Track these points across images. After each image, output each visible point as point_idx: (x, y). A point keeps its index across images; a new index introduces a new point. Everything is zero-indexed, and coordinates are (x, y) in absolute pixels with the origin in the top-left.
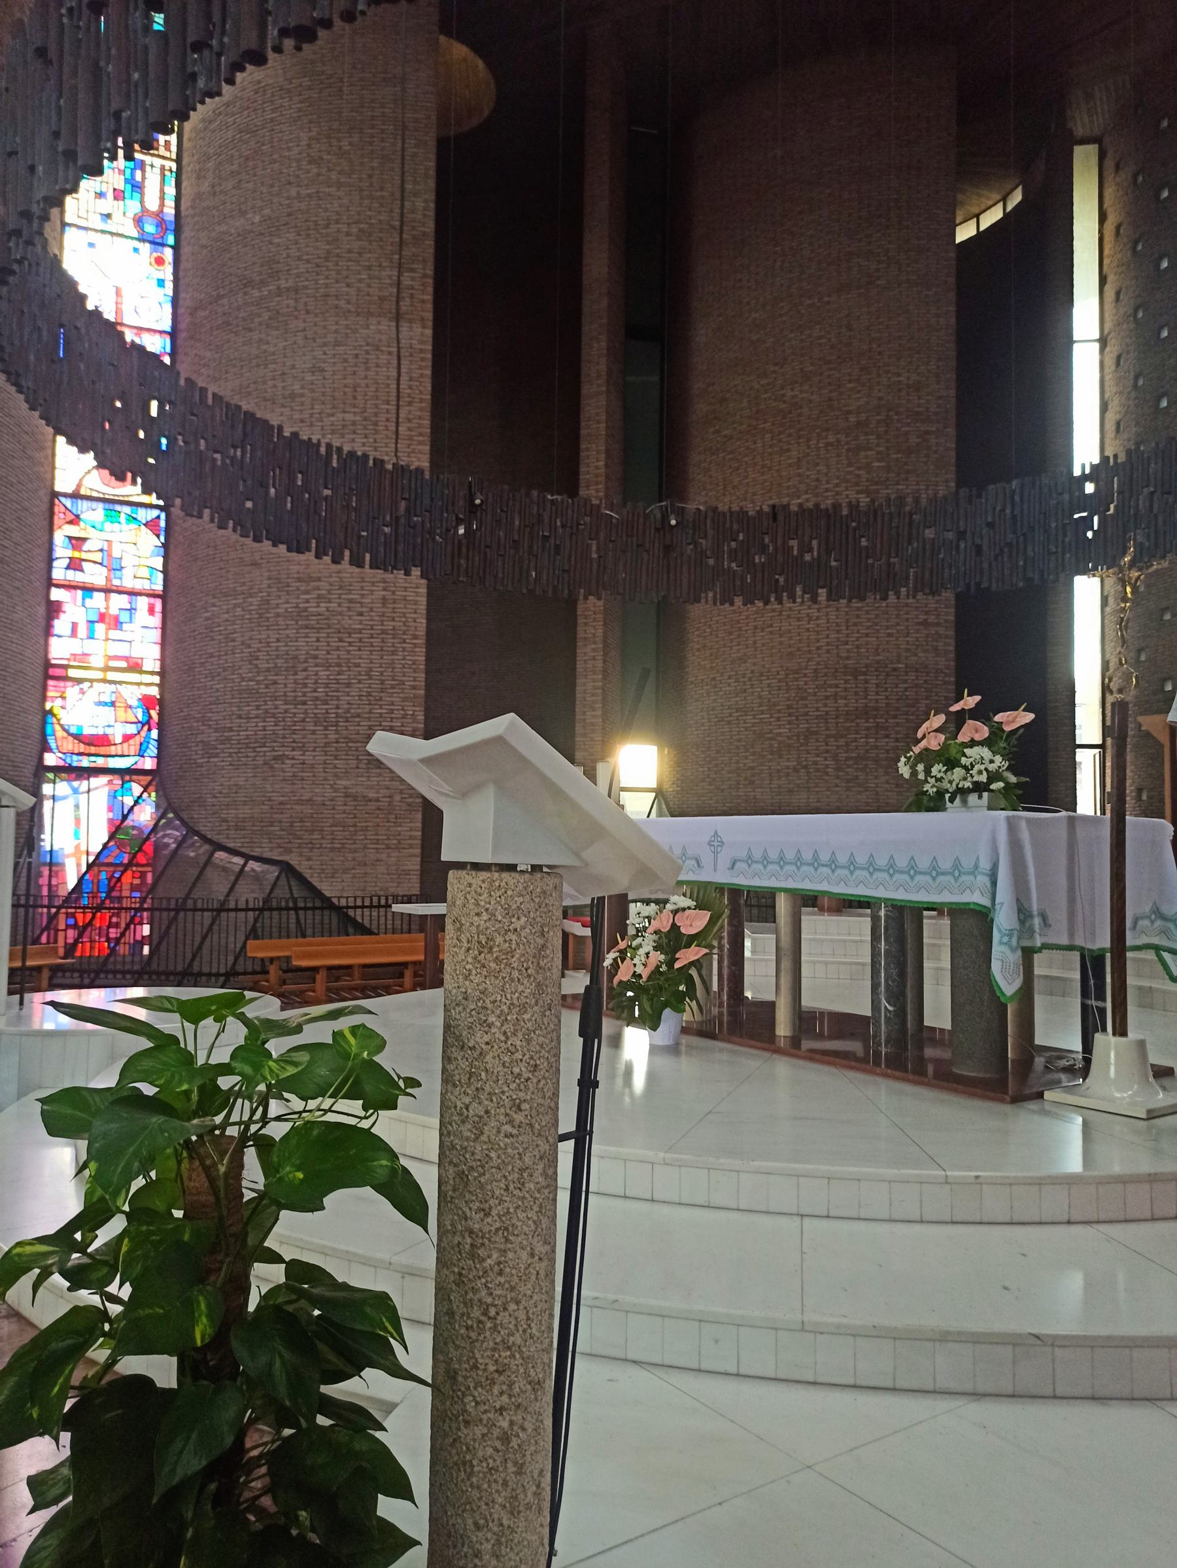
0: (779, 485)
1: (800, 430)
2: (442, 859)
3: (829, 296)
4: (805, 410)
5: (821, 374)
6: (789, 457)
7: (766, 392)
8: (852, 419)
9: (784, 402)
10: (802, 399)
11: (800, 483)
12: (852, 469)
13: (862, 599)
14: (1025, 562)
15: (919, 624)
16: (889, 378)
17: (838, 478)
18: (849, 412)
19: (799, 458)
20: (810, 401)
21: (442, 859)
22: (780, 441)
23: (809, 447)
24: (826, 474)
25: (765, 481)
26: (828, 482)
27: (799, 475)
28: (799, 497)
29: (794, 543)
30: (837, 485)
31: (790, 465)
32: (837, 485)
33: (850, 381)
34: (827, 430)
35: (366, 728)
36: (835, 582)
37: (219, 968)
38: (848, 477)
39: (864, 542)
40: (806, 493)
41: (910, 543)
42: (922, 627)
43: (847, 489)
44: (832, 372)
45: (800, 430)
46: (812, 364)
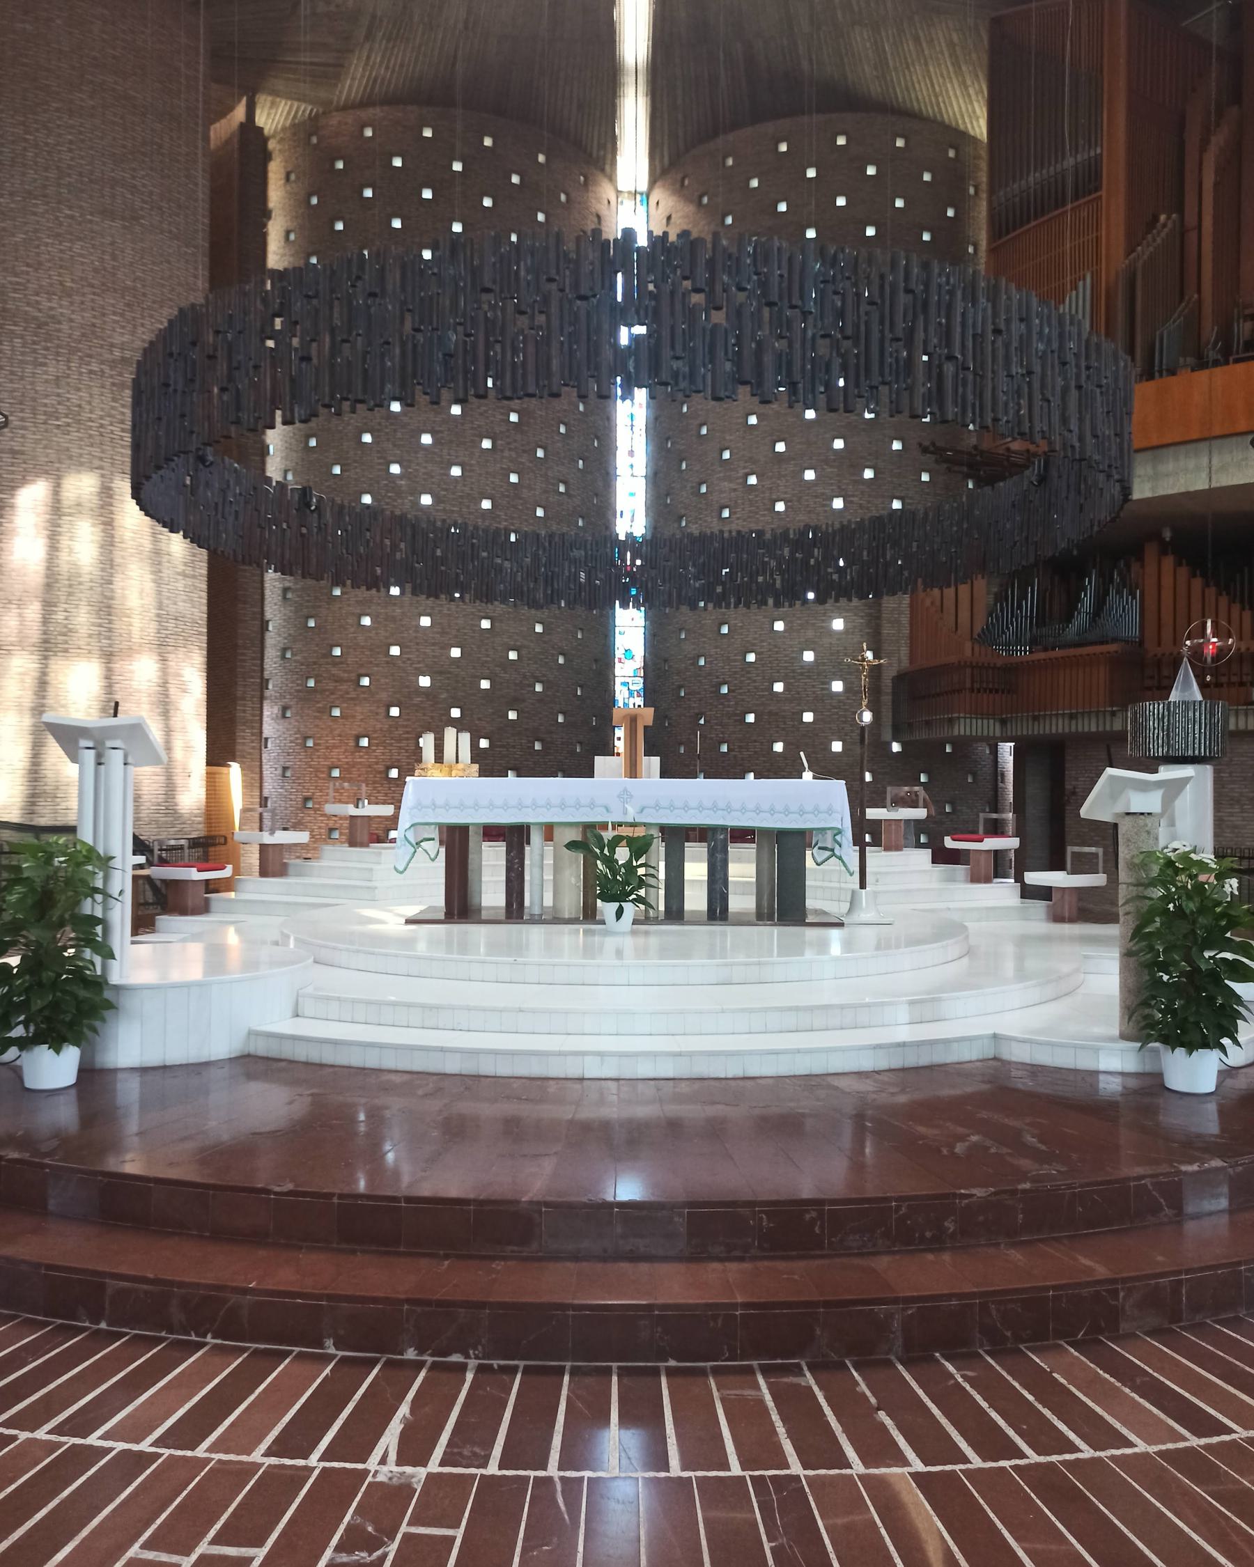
0: (34, 400)
1: (58, 346)
2: (597, 758)
3: (91, 214)
4: (65, 326)
5: (84, 295)
6: (46, 373)
7: (15, 291)
8: (117, 353)
9: (40, 311)
10: (62, 314)
11: (59, 403)
12: (117, 405)
13: (437, 597)
14: (552, 591)
15: (179, 574)
16: (152, 323)
17: (102, 409)
18: (112, 345)
19: (58, 377)
20: (71, 320)
21: (597, 758)
22: (35, 351)
23: (69, 368)
24: (89, 403)
25: (14, 390)
26: (91, 412)
27: (58, 395)
28: (57, 419)
29: (387, 542)
30: (101, 418)
31: (47, 381)
32: (101, 418)
33: (114, 313)
34: (90, 356)
35: (1036, 723)
36: (418, 581)
38: (113, 412)
39: (439, 553)
40: (67, 416)
41: (473, 561)
42: (181, 577)
43: (111, 424)
44: (96, 297)
45: (58, 346)
46: (73, 281)
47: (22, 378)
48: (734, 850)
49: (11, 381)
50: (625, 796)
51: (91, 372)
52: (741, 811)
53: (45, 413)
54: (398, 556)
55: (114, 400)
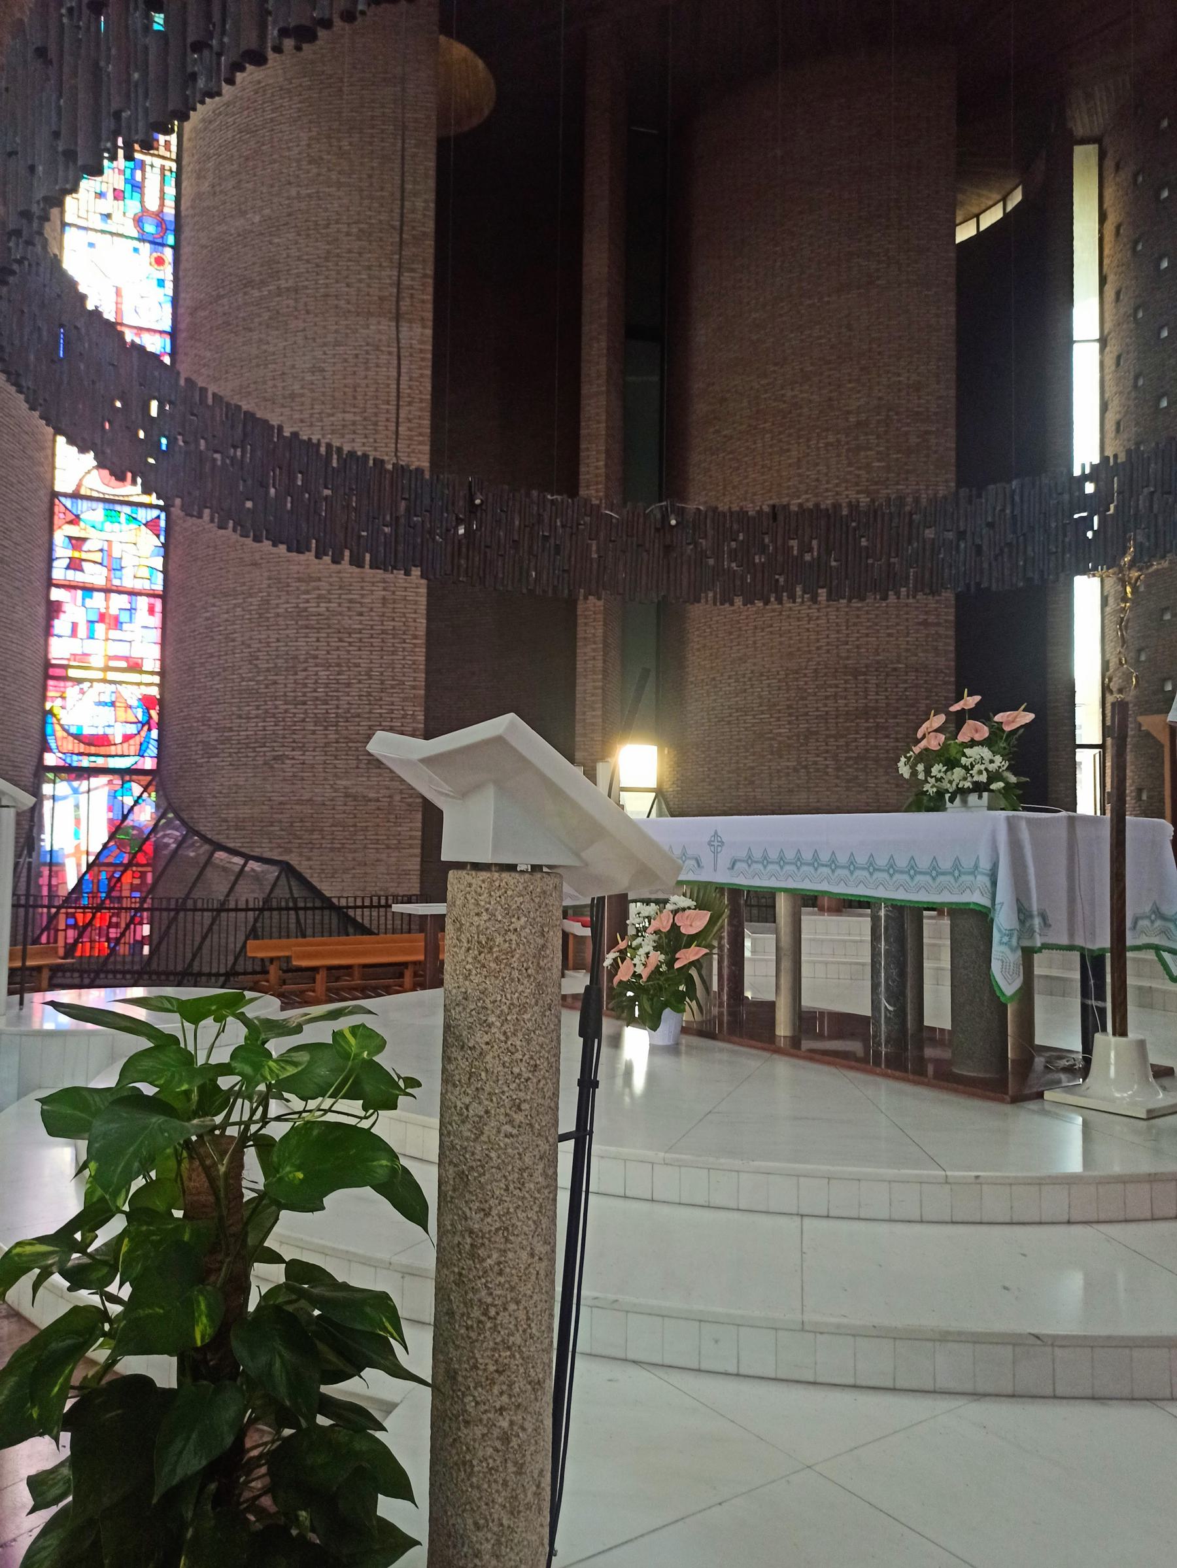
0: (779, 485)
1: (800, 430)
2: (442, 859)
4: (805, 410)
6: (789, 457)
8: (852, 419)
9: (784, 402)
10: (802, 399)
11: (800, 483)
12: (852, 469)
13: (862, 599)
15: (919, 624)
16: (889, 378)
17: (838, 478)
18: (849, 412)
20: (810, 401)
21: (442, 859)
22: (780, 441)
23: (809, 447)
24: (826, 474)
25: (765, 481)
26: (828, 482)
27: (799, 475)
28: (799, 497)
29: (794, 543)
30: (837, 485)
32: (837, 485)
33: (850, 381)
34: (827, 430)
35: (366, 728)
36: (835, 582)
37: (219, 968)
38: (848, 477)
40: (806, 493)
41: (910, 543)
43: (847, 489)
44: (832, 372)
45: (800, 430)
47: (770, 469)
48: (244, 907)
49: (763, 474)
50: (716, 844)
51: (827, 444)
52: (778, 863)
53: (788, 495)
54: (808, 557)
55: (850, 465)
